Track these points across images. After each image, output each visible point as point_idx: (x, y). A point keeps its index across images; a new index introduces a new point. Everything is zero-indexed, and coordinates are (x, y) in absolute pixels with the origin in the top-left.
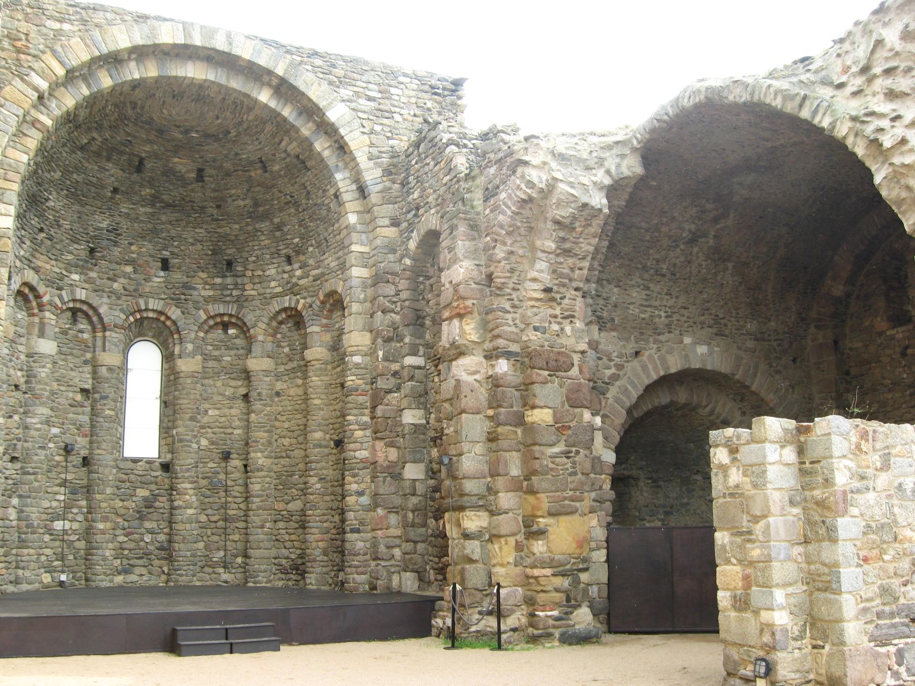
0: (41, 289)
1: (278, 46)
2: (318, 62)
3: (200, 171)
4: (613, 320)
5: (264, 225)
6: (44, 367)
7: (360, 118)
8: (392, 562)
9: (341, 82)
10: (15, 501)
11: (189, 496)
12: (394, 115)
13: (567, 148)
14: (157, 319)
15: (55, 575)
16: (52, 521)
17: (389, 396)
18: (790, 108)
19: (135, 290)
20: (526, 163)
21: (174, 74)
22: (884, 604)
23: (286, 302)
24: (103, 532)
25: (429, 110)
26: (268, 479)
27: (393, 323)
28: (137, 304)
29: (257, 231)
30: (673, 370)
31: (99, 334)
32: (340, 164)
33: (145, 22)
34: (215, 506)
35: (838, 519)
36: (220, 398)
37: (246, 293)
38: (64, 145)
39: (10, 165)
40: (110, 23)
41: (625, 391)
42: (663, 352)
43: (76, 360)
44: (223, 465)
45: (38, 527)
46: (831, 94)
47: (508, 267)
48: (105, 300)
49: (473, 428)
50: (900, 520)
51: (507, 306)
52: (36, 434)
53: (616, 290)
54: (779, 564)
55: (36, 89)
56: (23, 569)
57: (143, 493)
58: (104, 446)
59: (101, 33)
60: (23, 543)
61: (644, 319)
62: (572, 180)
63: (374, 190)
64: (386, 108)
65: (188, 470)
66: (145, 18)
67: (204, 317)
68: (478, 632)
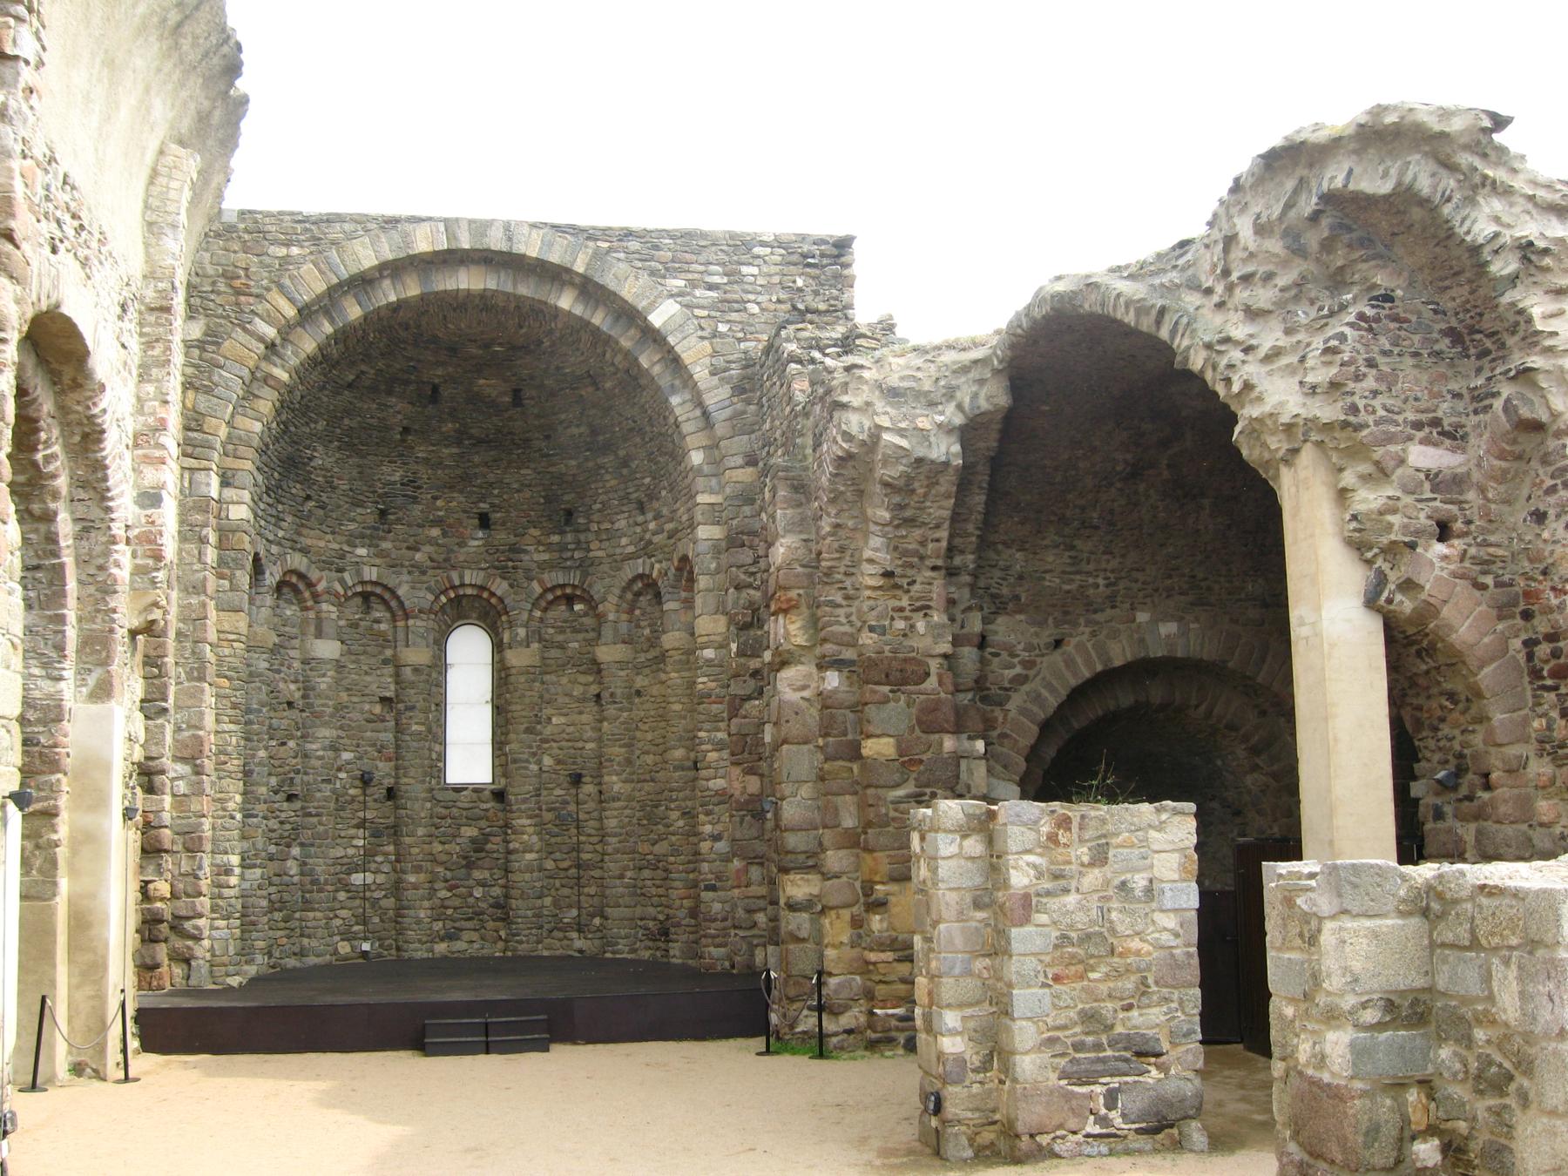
0: (314, 575)
1: (575, 230)
2: (634, 245)
3: (517, 393)
4: (1017, 598)
5: (605, 460)
6: (324, 675)
7: (697, 317)
8: (755, 932)
9: (670, 270)
10: (296, 851)
11: (527, 833)
12: (749, 305)
13: (902, 378)
14: (479, 597)
15: (356, 943)
17: (747, 705)
18: (1146, 325)
19: (447, 560)
20: (844, 406)
21: (441, 288)
22: (1087, 1034)
23: (640, 566)
24: (415, 887)
25: (800, 290)
26: (627, 812)
27: (751, 603)
28: (450, 579)
29: (600, 467)
30: (1118, 663)
31: (400, 624)
32: (677, 382)
33: (395, 228)
34: (565, 848)
35: (1014, 932)
36: (567, 700)
37: (591, 554)
38: (323, 388)
39: (240, 438)
40: (350, 237)
41: (1037, 698)
42: (1101, 637)
43: (373, 661)
44: (573, 791)
45: (326, 882)
46: (1198, 303)
47: (836, 545)
48: (405, 577)
49: (798, 762)
50: (1120, 928)
51: (839, 598)
52: (318, 763)
53: (1019, 555)
54: (951, 980)
55: (261, 339)
56: (309, 937)
57: (469, 832)
58: (412, 772)
60: (307, 905)
61: (1068, 592)
62: (903, 425)
63: (719, 416)
64: (736, 297)
65: (525, 801)
67: (538, 590)
68: (804, 1032)
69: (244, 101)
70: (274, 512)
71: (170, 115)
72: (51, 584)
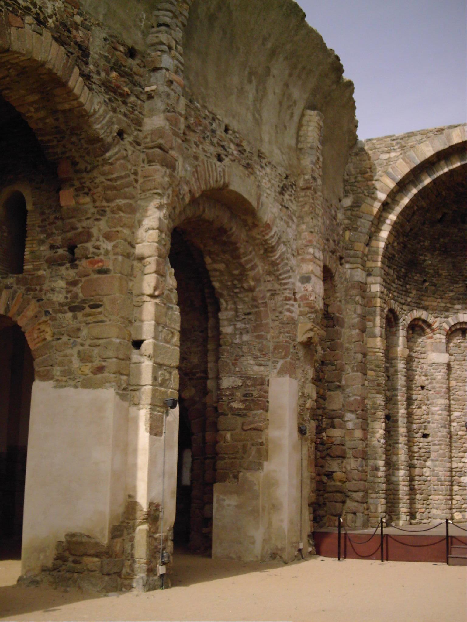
6: (440, 372)
16: (460, 477)
33: (442, 133)
38: (423, 224)
59: (414, 151)
66: (440, 131)
69: (350, 84)
70: (404, 289)
71: (305, 96)
72: (256, 321)
